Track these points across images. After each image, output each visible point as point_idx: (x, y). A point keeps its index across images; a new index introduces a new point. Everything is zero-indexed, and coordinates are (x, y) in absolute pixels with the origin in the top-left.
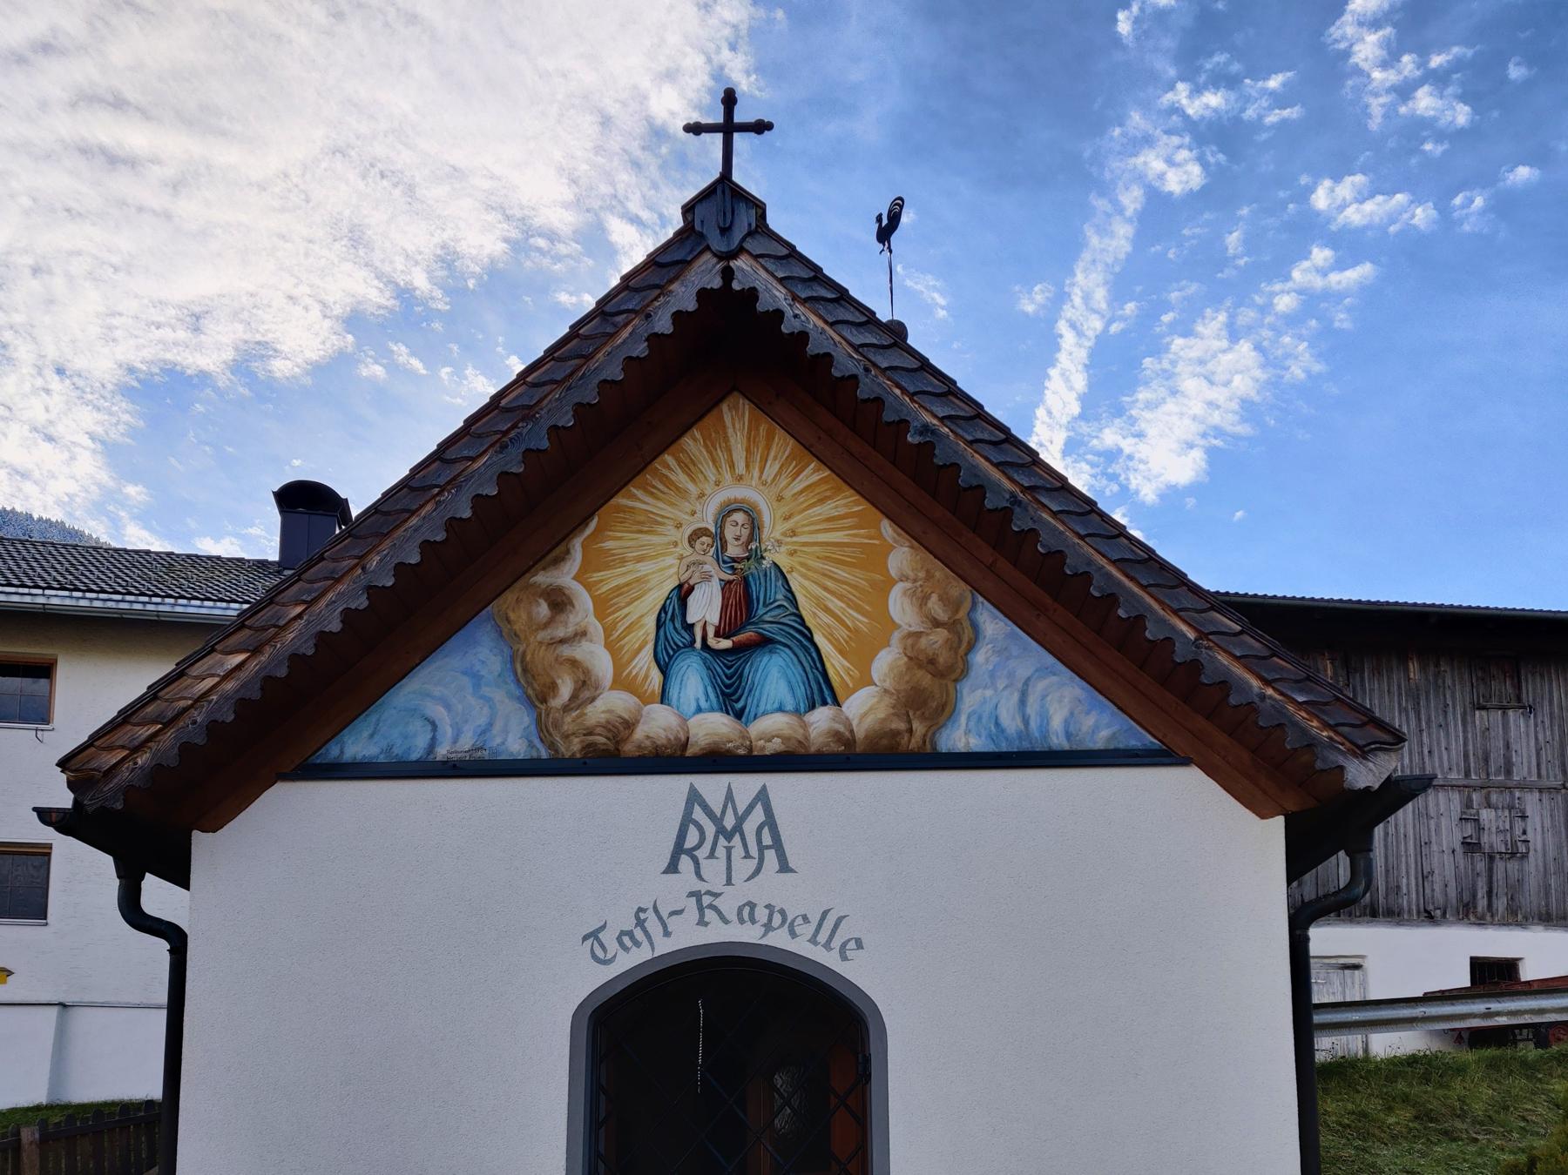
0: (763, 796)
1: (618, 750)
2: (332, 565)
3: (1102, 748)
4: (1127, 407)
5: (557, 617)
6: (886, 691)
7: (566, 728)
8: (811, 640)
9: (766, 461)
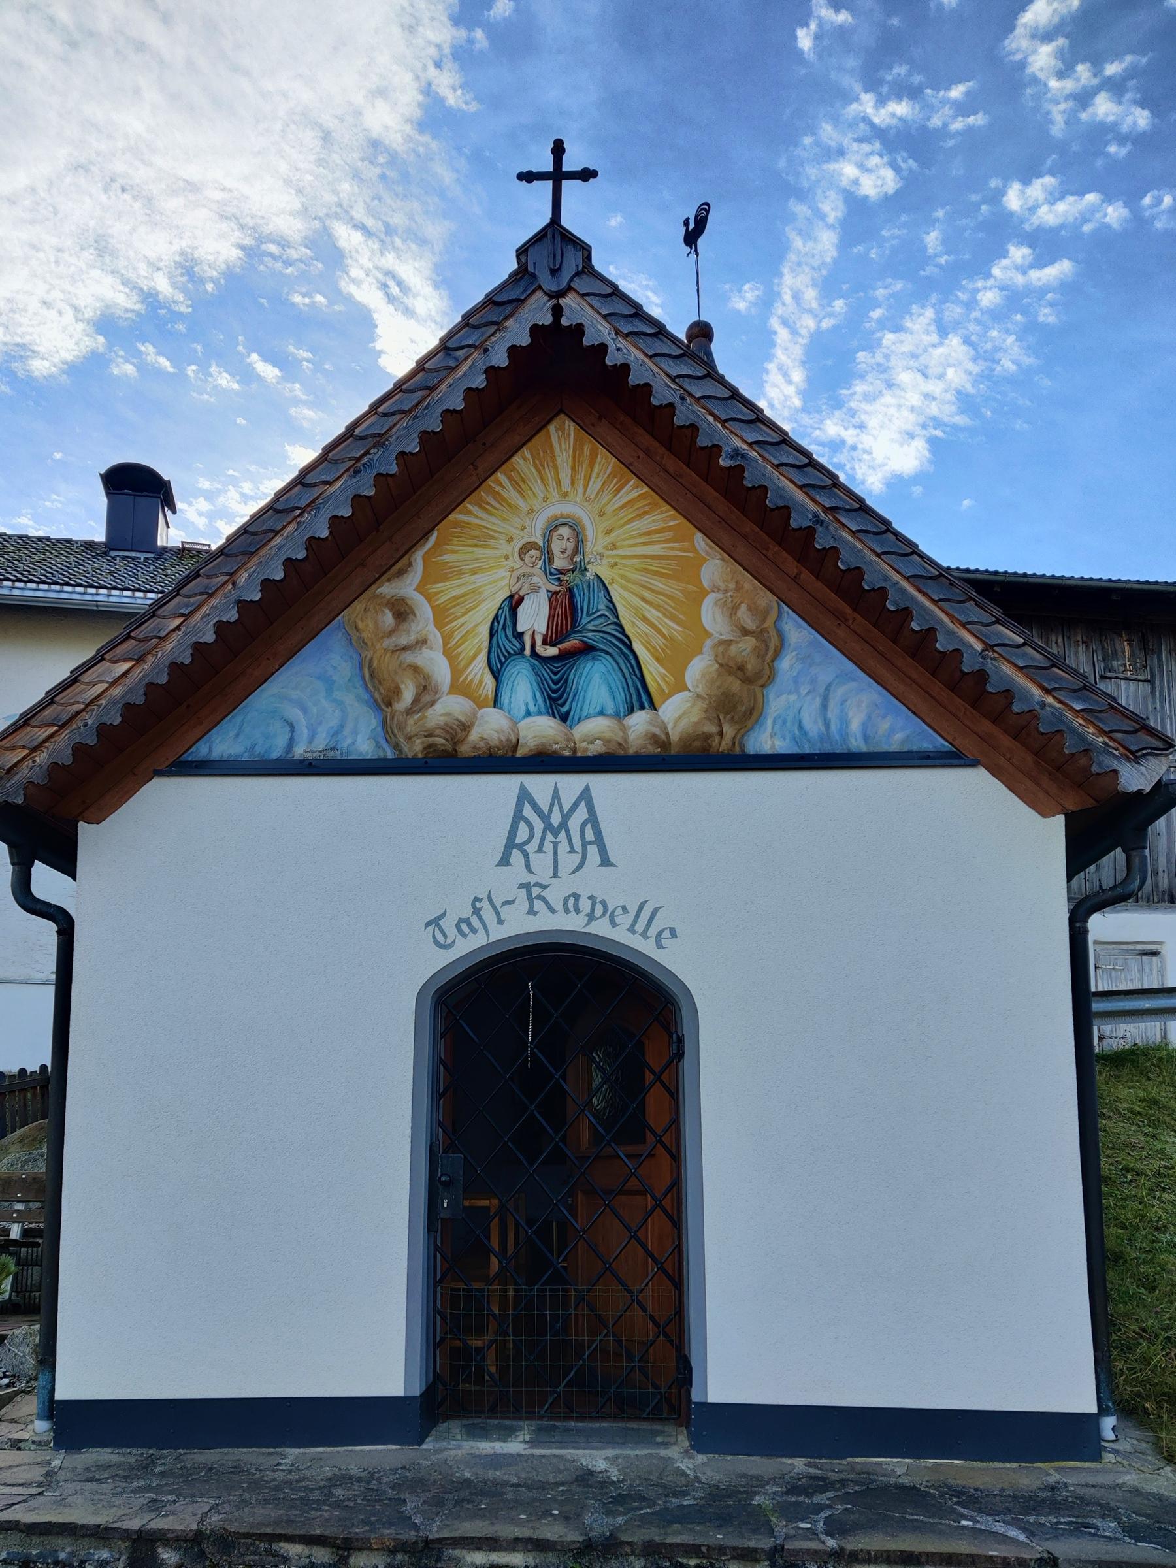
0: (586, 796)
1: (455, 750)
2: (205, 581)
3: (897, 750)
4: (846, 400)
5: (401, 627)
6: (698, 696)
7: (409, 729)
8: (630, 648)
9: (590, 478)
